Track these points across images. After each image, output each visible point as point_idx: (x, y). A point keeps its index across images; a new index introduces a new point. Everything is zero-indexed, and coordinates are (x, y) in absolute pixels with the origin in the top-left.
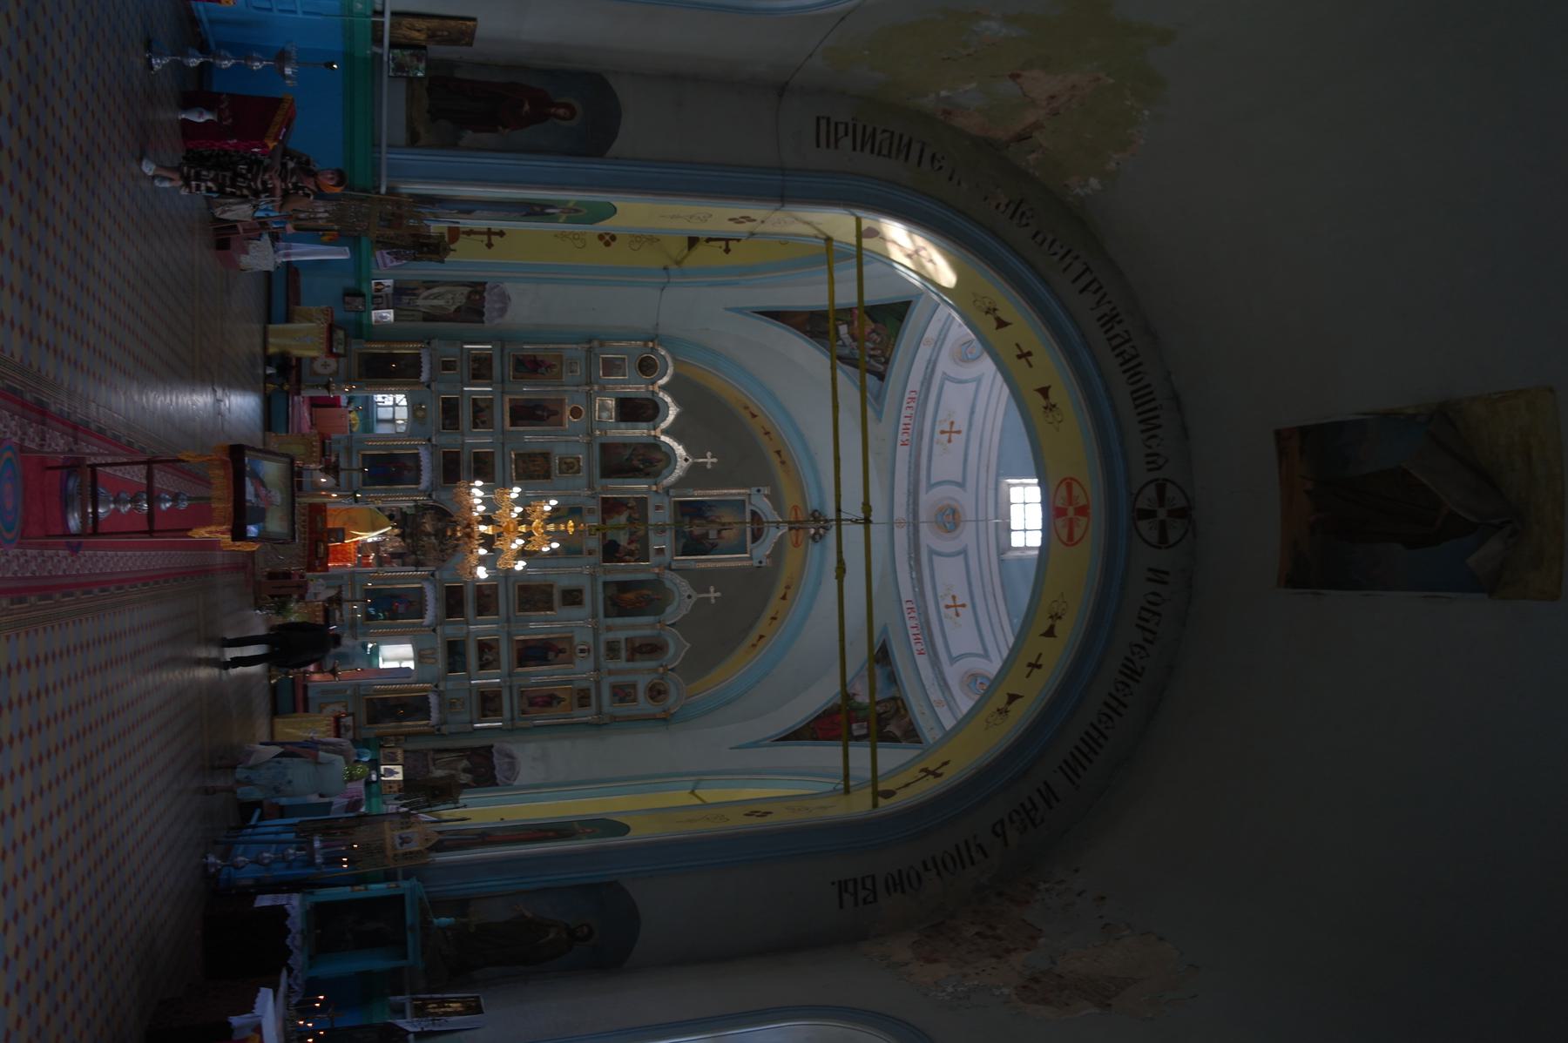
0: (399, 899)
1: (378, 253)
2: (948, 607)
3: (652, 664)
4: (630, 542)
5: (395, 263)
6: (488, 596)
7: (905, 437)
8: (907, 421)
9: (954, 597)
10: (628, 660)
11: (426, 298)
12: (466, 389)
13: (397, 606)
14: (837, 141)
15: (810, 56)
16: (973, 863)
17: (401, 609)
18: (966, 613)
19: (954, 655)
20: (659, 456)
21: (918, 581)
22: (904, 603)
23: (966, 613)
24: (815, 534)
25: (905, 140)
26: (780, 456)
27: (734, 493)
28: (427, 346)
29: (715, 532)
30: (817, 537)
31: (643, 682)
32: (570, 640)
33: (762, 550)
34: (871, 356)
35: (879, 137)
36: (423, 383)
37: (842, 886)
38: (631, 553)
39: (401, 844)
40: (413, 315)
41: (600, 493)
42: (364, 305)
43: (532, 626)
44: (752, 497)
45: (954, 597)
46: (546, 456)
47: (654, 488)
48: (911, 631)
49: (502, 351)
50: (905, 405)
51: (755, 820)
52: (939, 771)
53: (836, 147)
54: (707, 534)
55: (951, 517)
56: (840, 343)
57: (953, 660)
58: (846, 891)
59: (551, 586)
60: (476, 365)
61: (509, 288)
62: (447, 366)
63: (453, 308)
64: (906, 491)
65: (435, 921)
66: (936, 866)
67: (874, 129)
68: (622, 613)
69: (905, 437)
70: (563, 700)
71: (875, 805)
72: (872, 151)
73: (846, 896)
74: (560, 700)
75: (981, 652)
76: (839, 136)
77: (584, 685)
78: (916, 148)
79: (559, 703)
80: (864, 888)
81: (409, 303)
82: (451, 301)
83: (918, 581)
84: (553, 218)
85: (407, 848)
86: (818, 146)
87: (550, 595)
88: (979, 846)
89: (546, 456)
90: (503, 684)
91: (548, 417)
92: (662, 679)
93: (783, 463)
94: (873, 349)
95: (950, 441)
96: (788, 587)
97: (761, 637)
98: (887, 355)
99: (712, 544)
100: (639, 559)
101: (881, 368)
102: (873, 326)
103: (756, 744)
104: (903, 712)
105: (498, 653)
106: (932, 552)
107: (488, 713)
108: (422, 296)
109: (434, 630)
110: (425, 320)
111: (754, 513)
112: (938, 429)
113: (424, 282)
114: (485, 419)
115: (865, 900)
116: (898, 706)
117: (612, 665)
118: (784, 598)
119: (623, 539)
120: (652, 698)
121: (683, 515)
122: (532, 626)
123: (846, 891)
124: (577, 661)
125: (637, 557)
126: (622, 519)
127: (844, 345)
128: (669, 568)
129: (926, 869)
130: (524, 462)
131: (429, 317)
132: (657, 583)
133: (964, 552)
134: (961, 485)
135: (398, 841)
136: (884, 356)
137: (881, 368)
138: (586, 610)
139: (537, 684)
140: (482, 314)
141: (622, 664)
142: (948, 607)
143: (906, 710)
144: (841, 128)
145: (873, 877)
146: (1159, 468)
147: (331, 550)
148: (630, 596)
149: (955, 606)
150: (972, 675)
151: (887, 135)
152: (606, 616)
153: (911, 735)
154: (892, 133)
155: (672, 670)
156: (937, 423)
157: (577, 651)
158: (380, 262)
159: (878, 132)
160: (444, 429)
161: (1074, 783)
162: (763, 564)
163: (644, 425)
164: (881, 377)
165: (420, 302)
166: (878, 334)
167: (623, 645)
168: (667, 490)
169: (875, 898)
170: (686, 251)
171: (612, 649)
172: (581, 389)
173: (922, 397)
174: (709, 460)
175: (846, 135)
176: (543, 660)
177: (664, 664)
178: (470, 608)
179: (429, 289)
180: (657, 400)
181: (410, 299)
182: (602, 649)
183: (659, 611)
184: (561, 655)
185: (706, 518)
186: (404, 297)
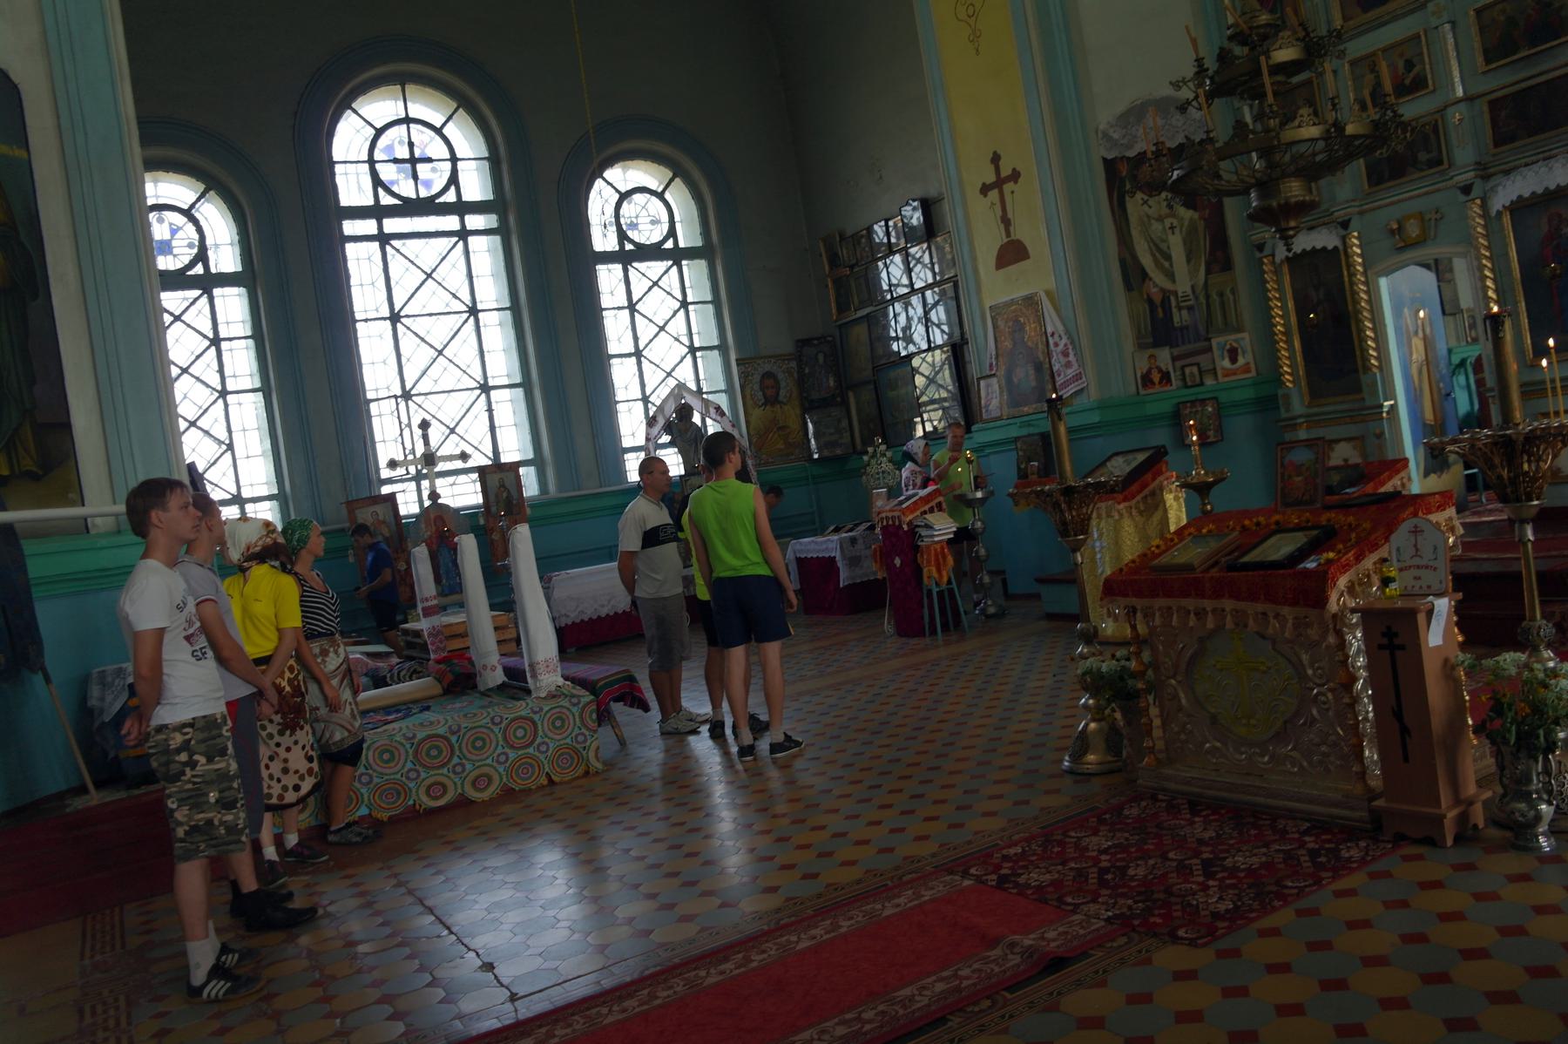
5: (1139, 375)
28: (1267, 251)
40: (1221, 295)
61: (1105, 116)
63: (1187, 214)
81: (1190, 308)
108: (1168, 285)
110: (1227, 266)
113: (1128, 286)
147: (826, 453)
158: (1072, 389)
165: (1183, 286)
179: (1144, 275)
181: (1180, 309)
186: (1176, 319)
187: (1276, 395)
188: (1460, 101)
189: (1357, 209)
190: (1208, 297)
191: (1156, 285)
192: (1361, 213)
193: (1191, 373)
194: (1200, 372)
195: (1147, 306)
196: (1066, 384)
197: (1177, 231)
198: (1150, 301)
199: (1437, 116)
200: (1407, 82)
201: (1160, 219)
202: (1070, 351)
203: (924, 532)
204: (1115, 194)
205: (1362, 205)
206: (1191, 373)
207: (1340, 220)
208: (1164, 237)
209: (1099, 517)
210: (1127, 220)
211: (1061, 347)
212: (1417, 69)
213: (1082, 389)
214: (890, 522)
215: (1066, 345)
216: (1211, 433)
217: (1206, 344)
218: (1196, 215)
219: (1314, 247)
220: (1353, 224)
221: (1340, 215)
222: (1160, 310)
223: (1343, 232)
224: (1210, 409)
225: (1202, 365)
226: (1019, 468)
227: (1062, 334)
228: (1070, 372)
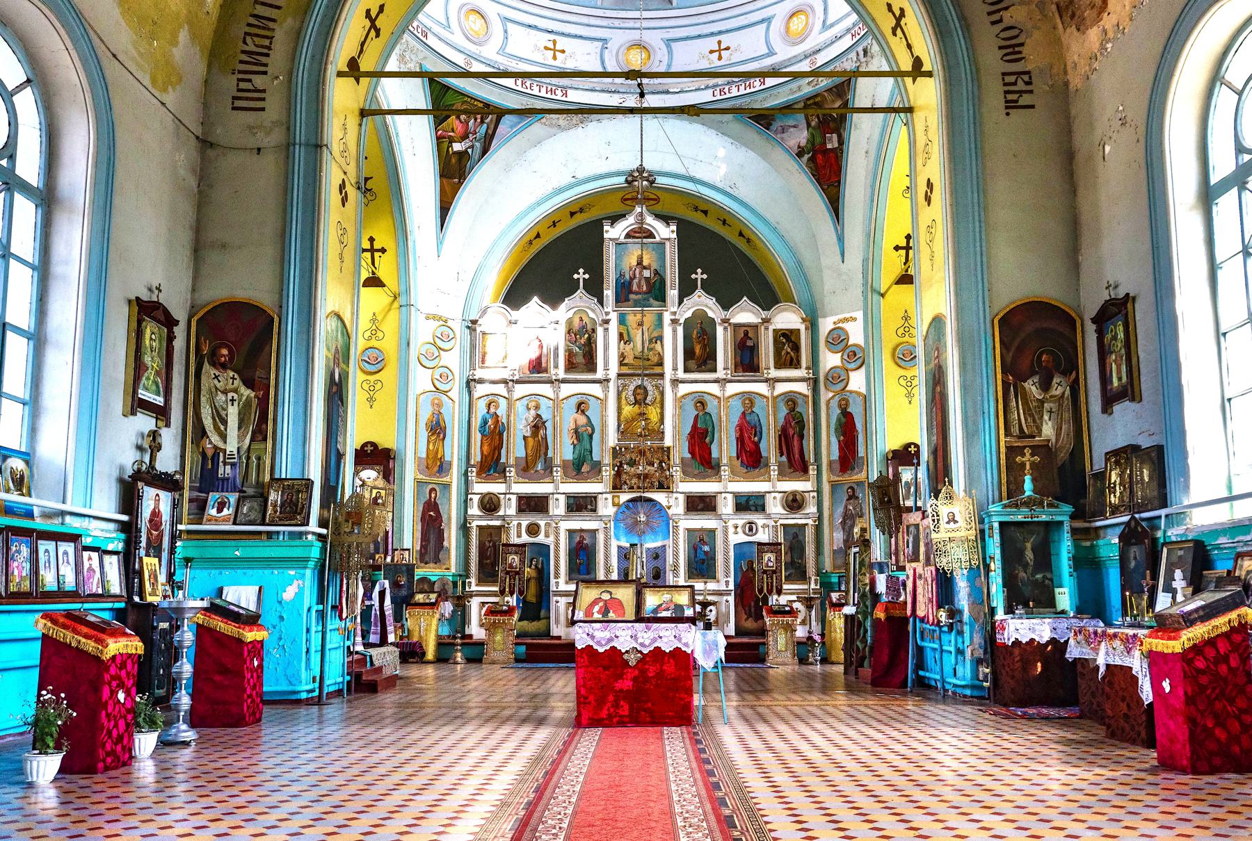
0: (1001, 524)
2: (720, 58)
7: (559, 92)
8: (543, 90)
9: (711, 52)
14: (257, 91)
15: (163, 104)
18: (726, 40)
19: (767, 51)
22: (715, 99)
23: (726, 40)
25: (252, 21)
26: (575, 213)
30: (651, 178)
34: (482, 122)
35: (251, 48)
37: (1011, 105)
39: (956, 522)
40: (259, 459)
45: (711, 52)
48: (742, 92)
50: (528, 91)
51: (937, 196)
52: (898, 13)
53: (264, 91)
56: (470, 151)
57: (771, 53)
66: (999, 11)
67: (243, 52)
71: (929, 74)
72: (267, 55)
73: (1021, 103)
75: (765, 25)
76: (252, 88)
78: (260, 10)
80: (1015, 84)
84: (344, 376)
86: (263, 109)
93: (581, 210)
94: (476, 119)
95: (563, 51)
96: (696, 209)
97: (741, 234)
103: (841, 239)
104: (818, 99)
108: (221, 445)
116: (812, 103)
118: (705, 212)
121: (627, 300)
123: (1016, 101)
127: (472, 147)
129: (1000, 21)
142: (720, 58)
143: (816, 96)
144: (243, 85)
145: (1004, 74)
148: (698, 349)
149: (720, 50)
151: (249, 40)
153: (843, 86)
154: (246, 34)
156: (546, 62)
159: (247, 48)
165: (232, 446)
170: (385, 288)
174: (581, 275)
175: (250, 81)
185: (632, 279)
190: (248, 458)
191: (211, 442)
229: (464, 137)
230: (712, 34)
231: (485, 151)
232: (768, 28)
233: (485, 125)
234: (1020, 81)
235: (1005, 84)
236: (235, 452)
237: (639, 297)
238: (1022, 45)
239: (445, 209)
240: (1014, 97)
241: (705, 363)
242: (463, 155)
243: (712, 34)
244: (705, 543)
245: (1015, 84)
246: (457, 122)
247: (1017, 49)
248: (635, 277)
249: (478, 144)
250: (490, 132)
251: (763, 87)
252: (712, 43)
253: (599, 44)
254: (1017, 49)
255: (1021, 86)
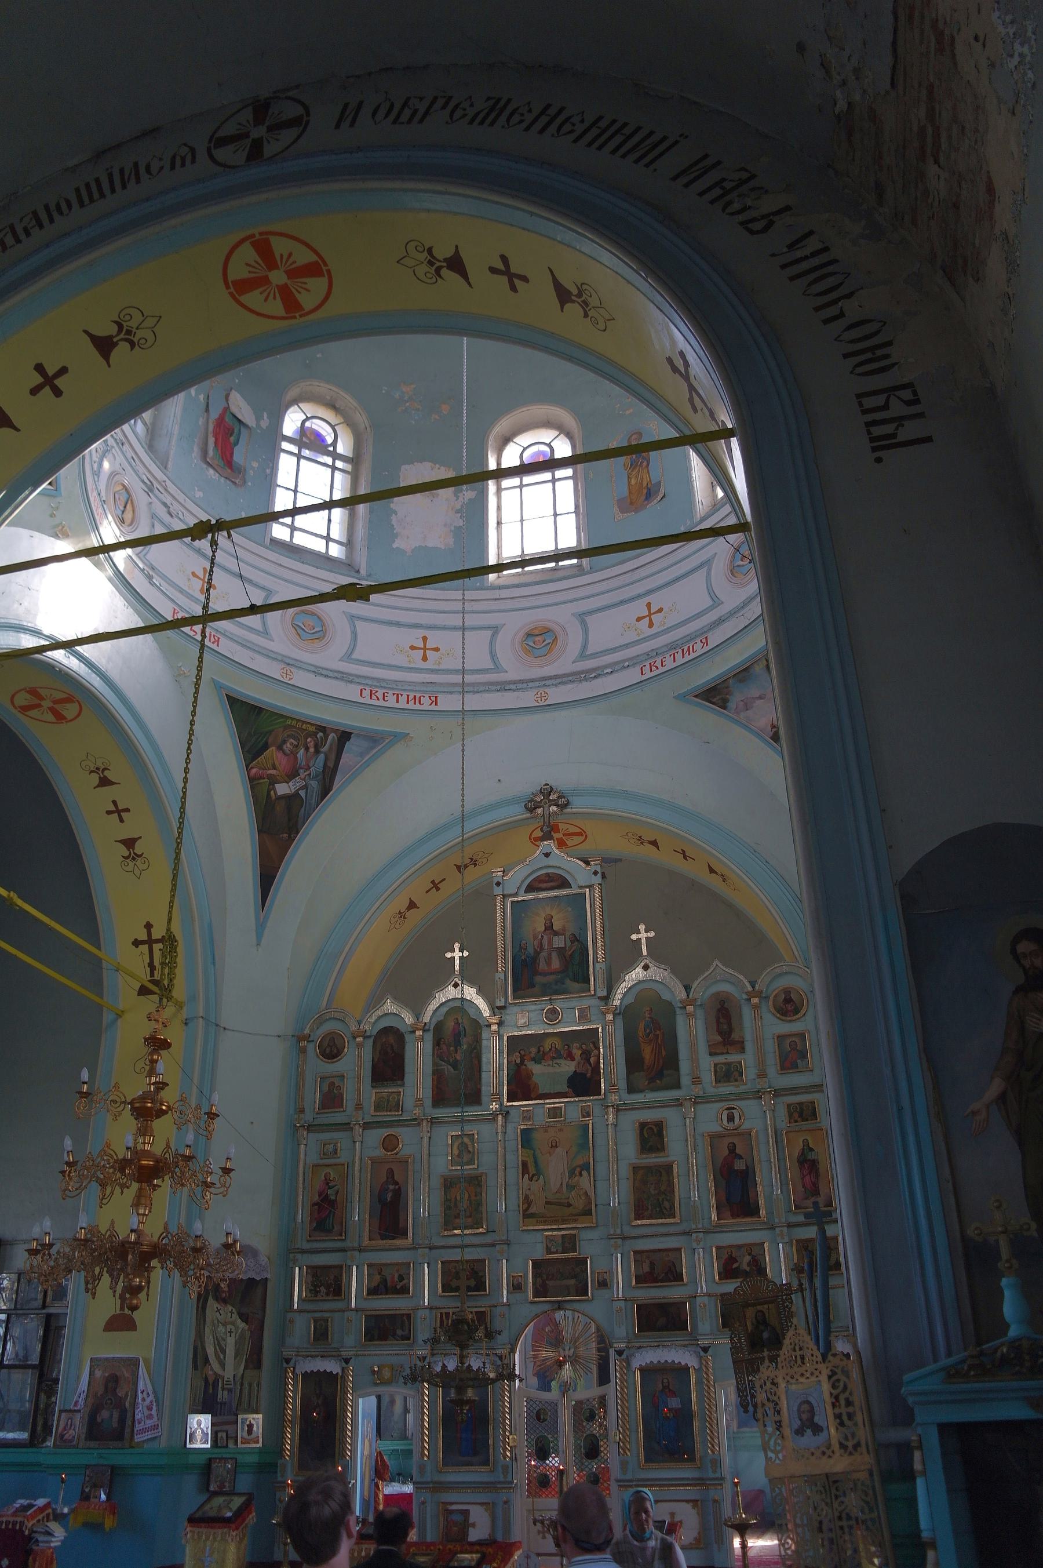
1: (138, 1438)
3: (747, 1013)
4: (570, 1057)
6: (652, 1264)
7: (426, 701)
8: (403, 700)
9: (639, 619)
10: (743, 1050)
11: (223, 1365)
12: (353, 1305)
13: (669, 1410)
16: (826, 249)
17: (674, 1403)
20: (450, 1024)
21: (616, 668)
22: (644, 678)
24: (557, 806)
27: (502, 916)
28: (292, 1364)
29: (555, 939)
31: (776, 1026)
32: (713, 1137)
33: (580, 874)
34: (317, 751)
36: (343, 1369)
37: (882, 445)
38: (586, 1055)
39: (817, 1429)
40: (250, 1385)
41: (501, 1104)
42: (225, 1460)
43: (695, 1196)
44: (506, 893)
45: (639, 619)
46: (449, 1184)
47: (494, 1028)
48: (680, 660)
49: (303, 1252)
50: (381, 703)
54: (561, 951)
55: (537, 638)
56: (302, 793)
57: (716, 602)
58: (894, 436)
59: (635, 1169)
60: (322, 1289)
62: (321, 1334)
63: (242, 1325)
64: (499, 694)
65: (1013, 1332)
66: (835, 302)
68: (672, 1061)
69: (426, 701)
70: (806, 1143)
73: (902, 436)
74: (807, 1148)
77: (782, 1113)
79: (811, 1150)
80: (886, 407)
81: (230, 1390)
82: (229, 1327)
83: (616, 668)
85: (826, 1416)
87: (649, 1169)
88: (791, 246)
89: (449, 1184)
90: (786, 1239)
91: (397, 1183)
92: (767, 998)
94: (307, 749)
95: (437, 649)
97: (712, 871)
98: (312, 729)
99: (572, 942)
100: (594, 1043)
101: (332, 736)
102: (273, 749)
105: (740, 1247)
106: (583, 656)
107: (832, 1262)
108: (219, 1371)
109: (705, 1350)
111: (530, 889)
112: (422, 665)
113: (195, 1367)
114: (396, 1276)
115: (909, 403)
117: (750, 1072)
118: (654, 843)
119: (568, 1068)
120: (796, 1011)
121: (532, 985)
122: (695, 1196)
123: (894, 436)
124: (746, 1126)
125: (591, 1045)
126: (537, 1070)
127: (305, 787)
128: (606, 999)
129: (842, 315)
130: (457, 1216)
131: (255, 1361)
132: (626, 1013)
133: (582, 617)
134: (495, 630)
135: (808, 1439)
136: (315, 734)
137: (332, 736)
138: (670, 1116)
139: (784, 1185)
140: (251, 1280)
141: (748, 1061)
142: (651, 625)
146: (193, 150)
148: (647, 1052)
149: (650, 615)
150: (732, 573)
152: (677, 1086)
155: (753, 985)
157: (731, 1126)
158: (147, 1436)
160: (409, 1339)
161: (676, 142)
162: (598, 868)
163: (408, 1048)
164: (345, 736)
165: (228, 1374)
166: (284, 742)
167: (721, 1059)
168: (495, 1009)
169: (904, 387)
171: (728, 1074)
172: (358, 1138)
173: (370, 682)
176: (746, 1177)
177: (745, 996)
178: (672, 1293)
179: (206, 1360)
180: (375, 1033)
181: (223, 1389)
182: (727, 1089)
183: (668, 1010)
184: (737, 1151)
185: (537, 953)
186: (220, 1396)
187: (277, 1463)
188: (426, 1308)
189: (354, 1352)
190: (242, 1384)
191: (212, 1369)
192: (357, 1356)
193: (222, 1437)
194: (227, 1437)
195: (203, 1384)
196: (143, 1431)
197: (233, 1335)
198: (206, 1380)
199: (411, 1312)
200: (398, 1287)
201: (225, 1324)
202: (154, 1407)
203: (41, 1538)
204: (202, 1300)
205: (357, 1351)
206: (222, 1437)
207: (345, 1357)
208: (225, 1337)
209: (215, 1539)
210: (204, 1321)
211: (148, 1402)
212: (404, 1282)
213: (156, 1437)
214: (18, 1527)
215: (151, 1402)
216: (227, 1484)
217: (233, 1418)
218: (247, 1327)
219: (325, 1370)
220: (352, 1362)
221: (345, 1354)
222: (211, 1387)
223: (344, 1365)
224: (229, 1466)
225: (229, 1432)
226: (83, 1491)
227: (150, 1393)
228: (150, 1423)
229: (292, 775)
230: (639, 596)
231: (325, 790)
232: (709, 573)
233: (322, 756)
234: (893, 401)
235: (865, 412)
236: (232, 1379)
237: (552, 977)
238: (889, 344)
239: (267, 878)
240: (888, 429)
241: (660, 1075)
242: (292, 799)
243: (639, 596)
244: (674, 1394)
245: (886, 407)
246: (280, 754)
247: (879, 353)
248: (542, 949)
249: (314, 783)
250: (331, 764)
251: (706, 649)
252: (639, 608)
253: (489, 633)
254: (879, 353)
255: (897, 408)
